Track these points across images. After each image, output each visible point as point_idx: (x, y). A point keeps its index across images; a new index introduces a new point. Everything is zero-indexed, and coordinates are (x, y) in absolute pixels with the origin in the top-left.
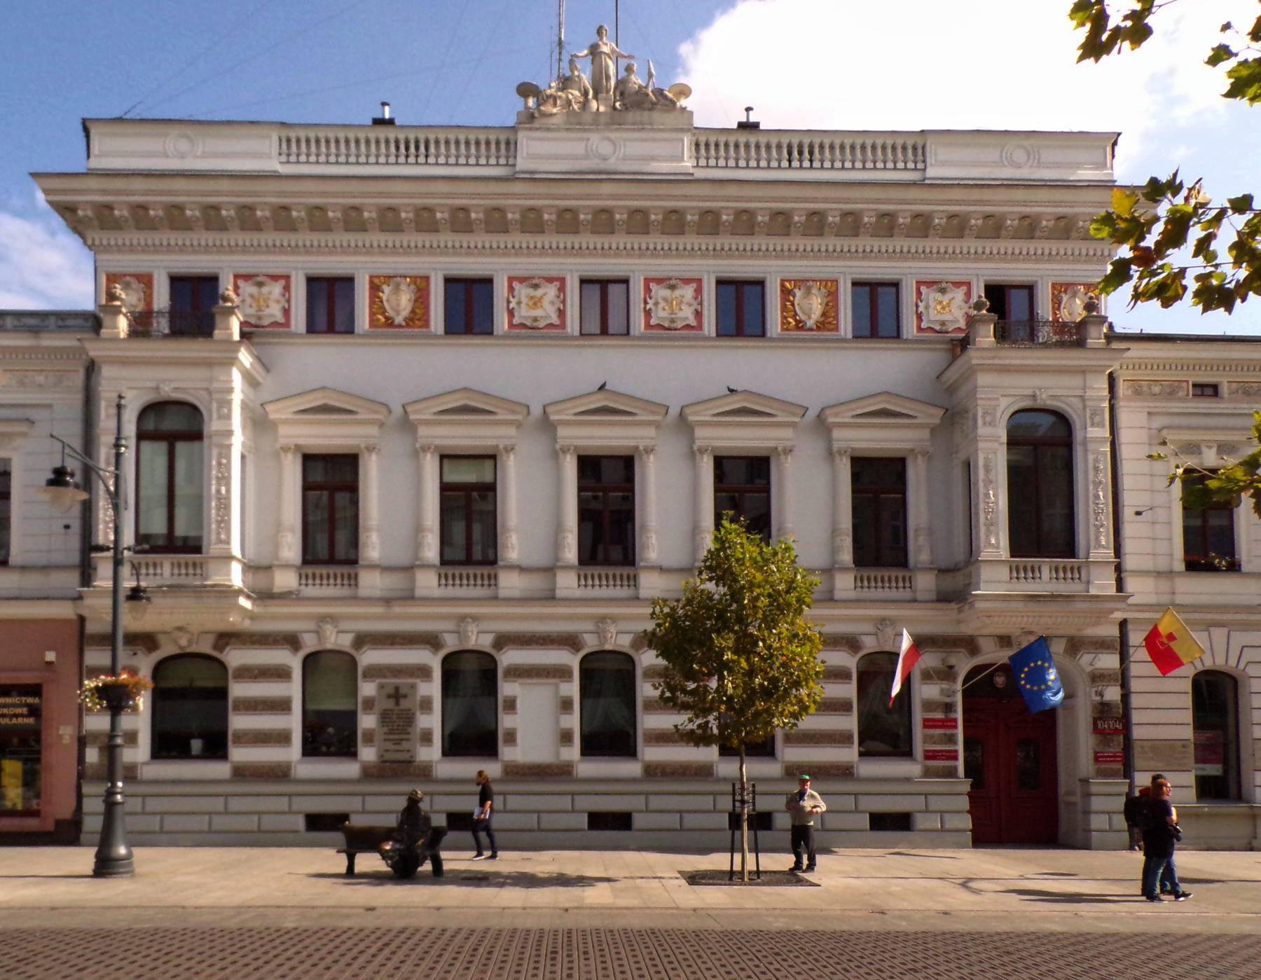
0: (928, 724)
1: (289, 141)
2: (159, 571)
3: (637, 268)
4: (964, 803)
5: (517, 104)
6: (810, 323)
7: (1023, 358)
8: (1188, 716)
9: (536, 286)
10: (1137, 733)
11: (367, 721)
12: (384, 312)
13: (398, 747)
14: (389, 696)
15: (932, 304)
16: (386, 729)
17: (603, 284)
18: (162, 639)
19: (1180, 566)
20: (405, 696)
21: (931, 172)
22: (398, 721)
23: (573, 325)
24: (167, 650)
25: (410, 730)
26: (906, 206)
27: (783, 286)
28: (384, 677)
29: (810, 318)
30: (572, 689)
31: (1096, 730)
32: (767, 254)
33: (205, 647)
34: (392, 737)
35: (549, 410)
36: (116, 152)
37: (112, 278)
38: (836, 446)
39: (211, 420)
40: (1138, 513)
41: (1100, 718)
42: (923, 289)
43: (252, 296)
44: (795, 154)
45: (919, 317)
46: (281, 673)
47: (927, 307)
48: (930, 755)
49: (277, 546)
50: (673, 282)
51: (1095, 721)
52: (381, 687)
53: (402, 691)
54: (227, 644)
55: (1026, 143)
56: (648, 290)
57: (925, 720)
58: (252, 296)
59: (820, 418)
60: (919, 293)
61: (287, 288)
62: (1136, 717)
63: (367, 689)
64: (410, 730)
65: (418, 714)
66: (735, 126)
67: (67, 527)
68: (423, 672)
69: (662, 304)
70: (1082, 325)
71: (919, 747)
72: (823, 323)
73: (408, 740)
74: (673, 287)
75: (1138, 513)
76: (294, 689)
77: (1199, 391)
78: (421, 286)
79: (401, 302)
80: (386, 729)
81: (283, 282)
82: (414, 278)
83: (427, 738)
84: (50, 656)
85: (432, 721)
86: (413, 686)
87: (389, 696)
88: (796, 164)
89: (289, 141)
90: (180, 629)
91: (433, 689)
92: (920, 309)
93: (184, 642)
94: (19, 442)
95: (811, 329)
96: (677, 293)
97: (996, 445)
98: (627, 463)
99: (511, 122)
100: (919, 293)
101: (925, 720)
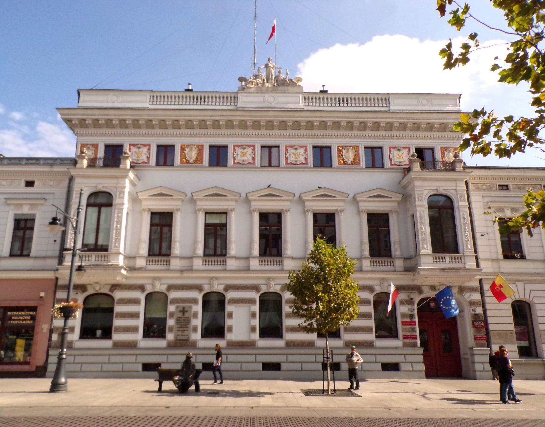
0: (404, 323)
1: (153, 97)
2: (90, 259)
3: (282, 142)
4: (421, 358)
5: (239, 84)
6: (349, 162)
7: (432, 175)
8: (511, 320)
9: (244, 149)
10: (491, 327)
11: (171, 322)
12: (185, 158)
13: (183, 334)
14: (180, 311)
15: (395, 155)
16: (178, 326)
17: (270, 148)
18: (89, 287)
19: (501, 257)
20: (187, 311)
21: (392, 108)
22: (184, 322)
23: (258, 163)
24: (90, 292)
25: (188, 326)
26: (383, 120)
27: (338, 148)
28: (179, 303)
29: (349, 160)
30: (256, 308)
31: (474, 326)
32: (332, 137)
33: (106, 291)
34: (180, 329)
35: (248, 195)
36: (88, 100)
37: (83, 146)
38: (361, 209)
39: (116, 198)
40: (482, 235)
41: (475, 321)
42: (236, 148)
43: (135, 152)
44: (341, 101)
45: (391, 160)
46: (136, 302)
47: (393, 156)
48: (405, 337)
49: (138, 248)
50: (296, 147)
51: (473, 322)
52: (177, 307)
53: (186, 309)
54: (115, 289)
55: (427, 98)
56: (287, 150)
57: (402, 322)
58: (135, 152)
59: (354, 198)
60: (390, 151)
61: (149, 149)
62: (490, 320)
63: (171, 308)
64: (188, 326)
65: (192, 319)
66: (319, 92)
67: (55, 241)
68: (195, 301)
69: (292, 155)
70: (453, 163)
71: (400, 334)
72: (354, 162)
73: (187, 330)
74: (296, 149)
75: (482, 235)
76: (141, 309)
77: (501, 188)
78: (200, 149)
79: (192, 154)
80: (178, 326)
81: (148, 147)
82: (198, 146)
83: (195, 329)
84: (42, 294)
85: (197, 322)
86: (190, 307)
87: (180, 311)
88: (341, 105)
89: (153, 97)
90: (96, 283)
91: (198, 308)
92: (391, 157)
93: (97, 288)
94: (40, 207)
95: (349, 164)
96: (298, 151)
97: (423, 209)
98: (279, 216)
99: (236, 90)
100: (390, 151)
101: (402, 322)
